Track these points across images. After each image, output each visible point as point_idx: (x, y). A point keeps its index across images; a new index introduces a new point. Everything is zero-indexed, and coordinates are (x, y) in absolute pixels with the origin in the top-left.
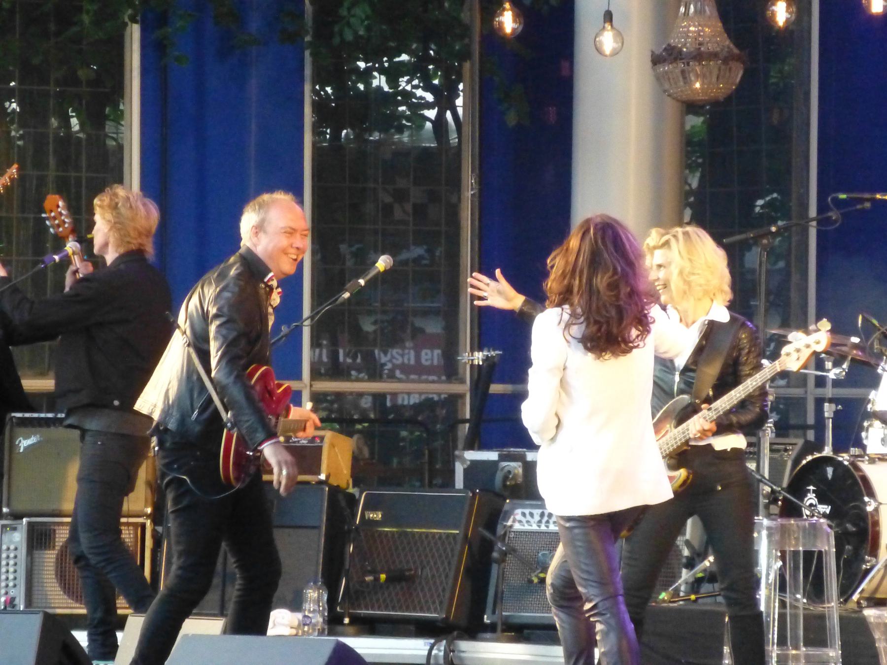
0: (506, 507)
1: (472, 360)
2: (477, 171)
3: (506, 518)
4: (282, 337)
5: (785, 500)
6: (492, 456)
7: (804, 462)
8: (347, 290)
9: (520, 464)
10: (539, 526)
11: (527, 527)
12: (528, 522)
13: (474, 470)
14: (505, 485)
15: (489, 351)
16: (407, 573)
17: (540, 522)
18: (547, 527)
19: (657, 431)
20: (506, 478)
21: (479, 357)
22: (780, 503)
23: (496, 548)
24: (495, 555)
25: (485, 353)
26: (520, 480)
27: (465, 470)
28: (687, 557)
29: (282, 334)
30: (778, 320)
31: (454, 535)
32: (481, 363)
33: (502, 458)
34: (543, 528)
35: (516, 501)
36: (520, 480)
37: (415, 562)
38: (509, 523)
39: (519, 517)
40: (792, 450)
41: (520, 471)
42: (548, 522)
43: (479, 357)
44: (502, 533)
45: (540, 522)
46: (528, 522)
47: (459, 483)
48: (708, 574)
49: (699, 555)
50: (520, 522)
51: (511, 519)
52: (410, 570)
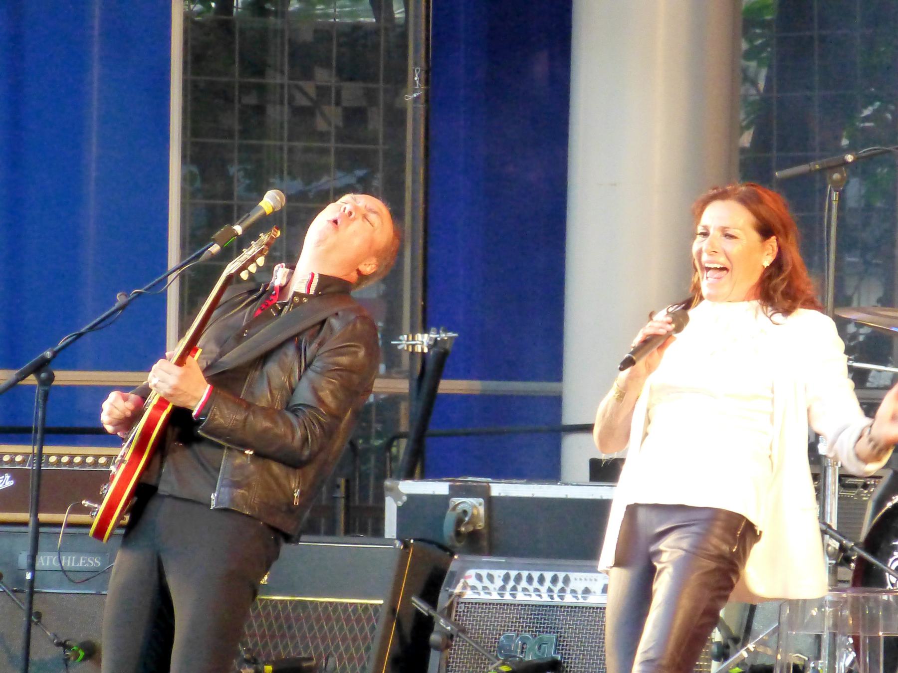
0: (453, 566)
1: (413, 346)
2: (423, 62)
3: (454, 582)
4: (117, 310)
5: (861, 560)
6: (440, 488)
7: (889, 505)
8: (215, 241)
9: (481, 500)
10: (502, 595)
11: (483, 596)
12: (485, 588)
13: (413, 508)
14: (458, 534)
15: (438, 333)
16: (305, 665)
17: (503, 588)
18: (513, 596)
19: (622, 460)
20: (459, 522)
21: (423, 341)
22: (853, 565)
23: (436, 628)
24: (434, 638)
25: (433, 335)
26: (481, 525)
27: (399, 509)
28: (718, 643)
29: (117, 305)
30: (873, 291)
31: (376, 608)
32: (426, 350)
33: (456, 491)
34: (507, 597)
35: (470, 558)
36: (481, 525)
37: (316, 648)
38: (457, 590)
39: (472, 581)
40: (875, 486)
41: (482, 510)
42: (514, 589)
43: (423, 341)
44: (447, 604)
45: (503, 588)
46: (537, 590)
47: (391, 528)
48: (748, 668)
49: (736, 640)
50: (473, 588)
51: (460, 585)
52: (310, 659)
